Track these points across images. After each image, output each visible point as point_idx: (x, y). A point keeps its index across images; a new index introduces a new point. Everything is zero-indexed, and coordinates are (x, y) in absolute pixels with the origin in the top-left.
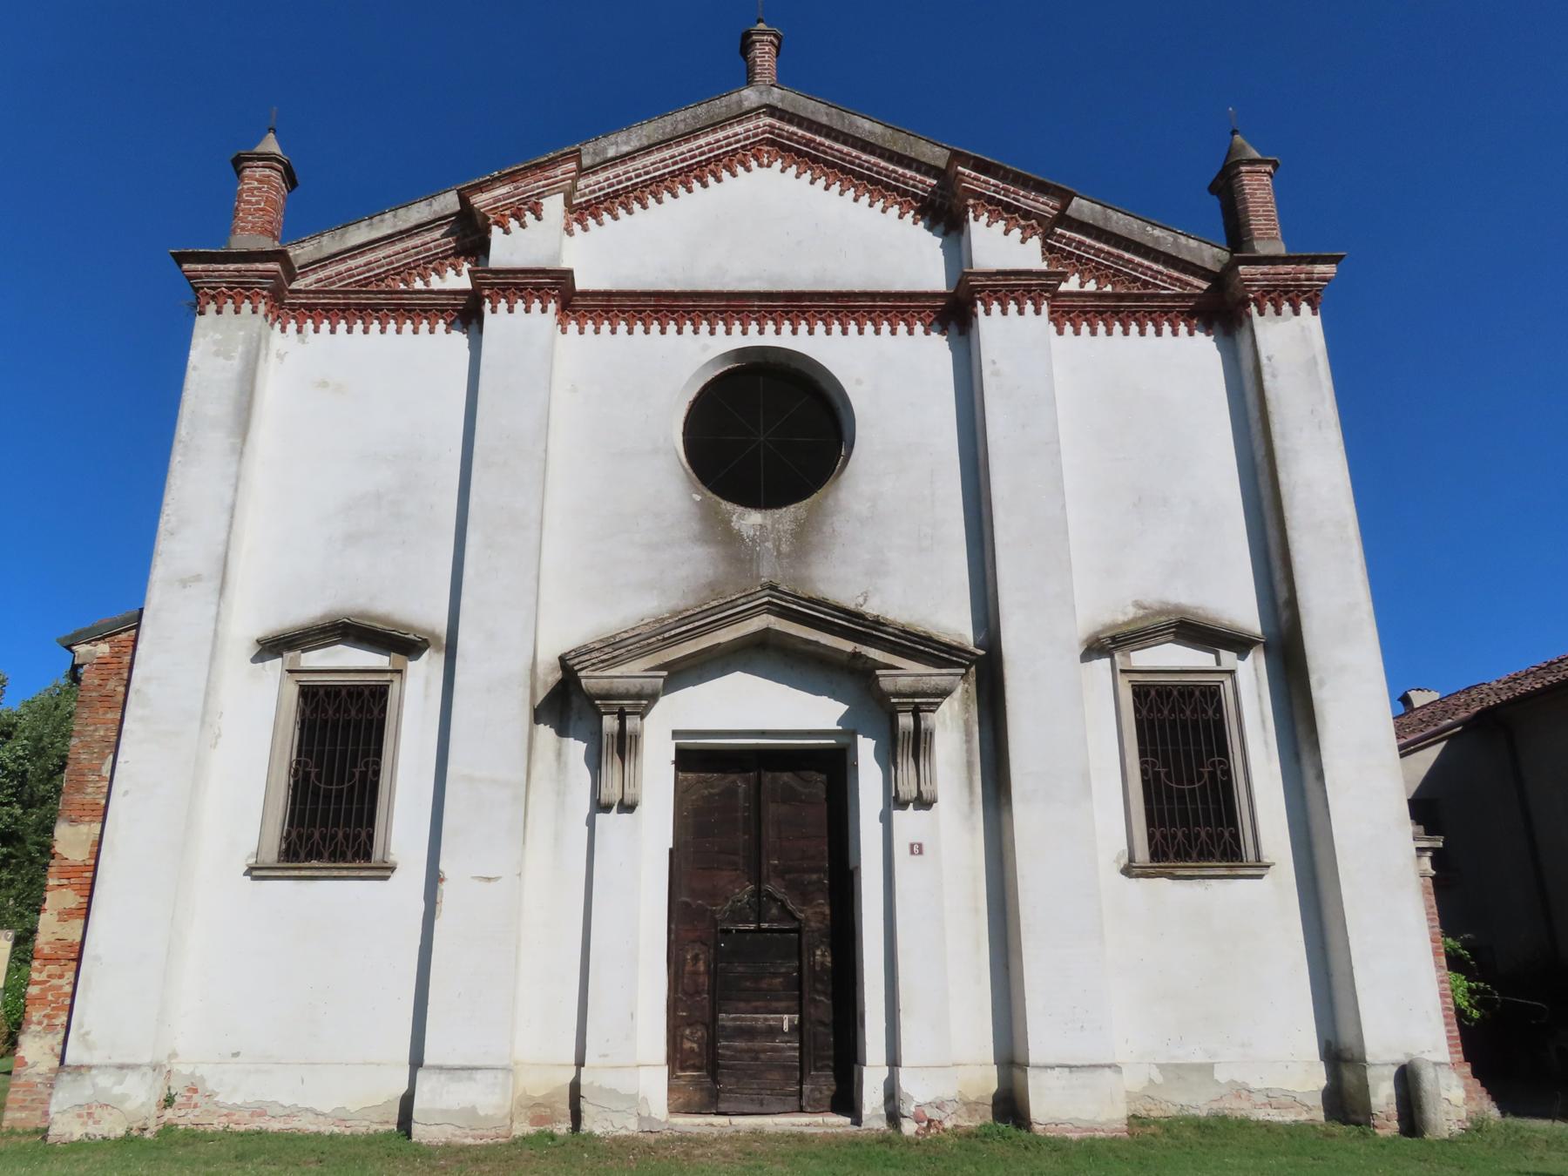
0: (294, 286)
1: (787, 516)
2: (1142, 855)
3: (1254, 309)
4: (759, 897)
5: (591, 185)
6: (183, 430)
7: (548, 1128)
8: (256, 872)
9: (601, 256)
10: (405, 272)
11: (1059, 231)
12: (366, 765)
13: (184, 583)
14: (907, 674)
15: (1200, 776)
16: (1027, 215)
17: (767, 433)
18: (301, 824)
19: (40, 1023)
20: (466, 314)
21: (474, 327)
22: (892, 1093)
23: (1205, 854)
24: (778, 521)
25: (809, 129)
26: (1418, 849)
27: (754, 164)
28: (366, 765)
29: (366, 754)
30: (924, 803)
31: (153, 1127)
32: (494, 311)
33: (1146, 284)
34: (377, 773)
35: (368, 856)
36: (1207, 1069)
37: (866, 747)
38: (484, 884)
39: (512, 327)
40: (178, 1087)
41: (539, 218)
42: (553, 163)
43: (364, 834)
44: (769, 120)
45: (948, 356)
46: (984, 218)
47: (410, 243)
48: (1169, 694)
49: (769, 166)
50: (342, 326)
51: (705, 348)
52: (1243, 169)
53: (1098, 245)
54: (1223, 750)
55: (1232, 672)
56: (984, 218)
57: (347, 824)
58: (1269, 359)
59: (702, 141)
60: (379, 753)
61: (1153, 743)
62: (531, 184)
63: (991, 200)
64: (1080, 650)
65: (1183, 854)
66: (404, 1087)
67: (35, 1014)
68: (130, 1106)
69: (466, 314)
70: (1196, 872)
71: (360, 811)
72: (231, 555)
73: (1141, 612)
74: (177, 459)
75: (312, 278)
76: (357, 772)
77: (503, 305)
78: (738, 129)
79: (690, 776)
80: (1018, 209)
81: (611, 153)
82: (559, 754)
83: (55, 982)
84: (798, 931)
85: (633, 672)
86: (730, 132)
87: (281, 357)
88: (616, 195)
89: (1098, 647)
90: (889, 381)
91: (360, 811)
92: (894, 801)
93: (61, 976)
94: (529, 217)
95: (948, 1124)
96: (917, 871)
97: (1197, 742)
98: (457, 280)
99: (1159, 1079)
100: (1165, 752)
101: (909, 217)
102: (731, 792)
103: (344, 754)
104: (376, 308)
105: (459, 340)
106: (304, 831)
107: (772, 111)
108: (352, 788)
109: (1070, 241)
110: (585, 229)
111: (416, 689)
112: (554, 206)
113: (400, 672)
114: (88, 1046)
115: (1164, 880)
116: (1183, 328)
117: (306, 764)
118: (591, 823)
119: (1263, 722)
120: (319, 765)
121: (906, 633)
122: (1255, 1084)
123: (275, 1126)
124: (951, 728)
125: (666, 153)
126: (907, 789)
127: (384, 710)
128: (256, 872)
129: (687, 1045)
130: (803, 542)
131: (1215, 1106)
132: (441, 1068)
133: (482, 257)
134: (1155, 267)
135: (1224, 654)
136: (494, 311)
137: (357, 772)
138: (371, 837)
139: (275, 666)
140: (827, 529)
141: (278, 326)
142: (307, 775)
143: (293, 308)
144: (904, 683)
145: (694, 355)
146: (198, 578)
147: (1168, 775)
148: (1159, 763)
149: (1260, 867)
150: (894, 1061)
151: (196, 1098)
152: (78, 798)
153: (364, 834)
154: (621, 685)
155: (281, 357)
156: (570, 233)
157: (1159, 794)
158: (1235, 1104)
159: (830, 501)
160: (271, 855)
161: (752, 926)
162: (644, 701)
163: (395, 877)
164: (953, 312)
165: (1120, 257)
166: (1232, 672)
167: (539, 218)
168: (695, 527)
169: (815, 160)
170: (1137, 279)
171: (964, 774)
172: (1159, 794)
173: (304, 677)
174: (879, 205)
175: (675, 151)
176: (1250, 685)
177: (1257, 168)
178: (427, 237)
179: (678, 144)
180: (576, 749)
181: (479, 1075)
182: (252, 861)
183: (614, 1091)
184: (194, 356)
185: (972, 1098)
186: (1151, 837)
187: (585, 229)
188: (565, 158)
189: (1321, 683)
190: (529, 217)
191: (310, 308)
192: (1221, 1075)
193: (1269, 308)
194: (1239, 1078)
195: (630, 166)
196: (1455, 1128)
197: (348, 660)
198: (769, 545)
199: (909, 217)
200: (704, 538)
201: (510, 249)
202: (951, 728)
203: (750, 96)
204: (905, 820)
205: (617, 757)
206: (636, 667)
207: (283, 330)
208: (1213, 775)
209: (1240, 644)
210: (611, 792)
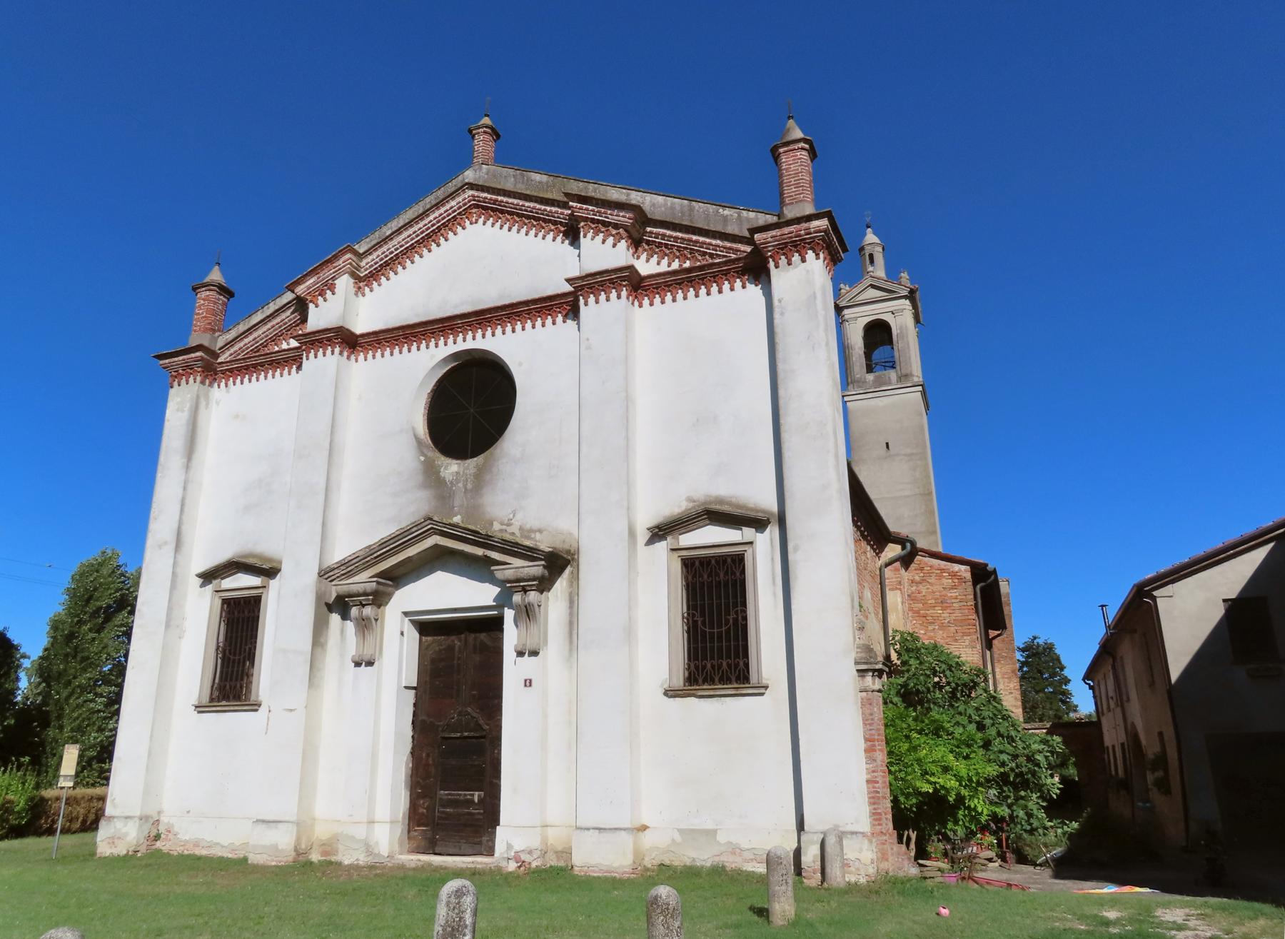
0: (219, 360)
1: (472, 463)
3: (772, 264)
5: (367, 263)
6: (162, 459)
7: (328, 858)
8: (671, 693)
9: (368, 311)
10: (275, 339)
11: (649, 229)
12: (736, 613)
13: (160, 547)
15: (727, 622)
16: (616, 226)
17: (472, 408)
18: (696, 659)
21: (763, 277)
23: (725, 680)
24: (467, 468)
25: (493, 193)
26: (858, 671)
28: (736, 613)
29: (735, 605)
31: (143, 849)
32: (586, 304)
33: (711, 256)
34: (745, 618)
35: (247, 699)
36: (712, 833)
37: (509, 615)
40: (162, 829)
42: (336, 257)
43: (741, 663)
44: (471, 192)
47: (274, 322)
48: (725, 561)
50: (726, 286)
51: (433, 356)
52: (781, 150)
53: (674, 234)
56: (590, 235)
57: (712, 658)
58: (780, 301)
59: (431, 218)
60: (744, 604)
62: (327, 273)
63: (593, 221)
65: (709, 680)
66: (796, 845)
68: (129, 839)
70: (712, 693)
71: (737, 647)
72: (184, 528)
73: (691, 505)
74: (159, 475)
75: (228, 353)
76: (731, 618)
77: (592, 299)
78: (453, 203)
79: (429, 638)
80: (609, 224)
81: (389, 233)
82: (342, 631)
86: (448, 206)
87: (217, 403)
88: (387, 264)
91: (737, 647)
95: (534, 865)
97: (727, 597)
99: (678, 838)
100: (703, 607)
101: (559, 239)
102: (450, 649)
103: (719, 606)
104: (262, 365)
105: (754, 291)
106: (233, 684)
107: (472, 186)
108: (728, 631)
109: (657, 235)
113: (751, 543)
114: (115, 806)
115: (693, 699)
116: (738, 283)
117: (694, 615)
119: (774, 579)
120: (703, 615)
122: (745, 845)
123: (204, 852)
125: (411, 231)
127: (743, 572)
128: (200, 708)
129: (421, 810)
130: (479, 481)
131: (717, 859)
134: (714, 242)
136: (586, 304)
137: (731, 618)
138: (747, 665)
139: (662, 547)
140: (494, 470)
141: (636, 303)
142: (695, 622)
143: (223, 372)
145: (424, 364)
146: (166, 543)
147: (704, 623)
148: (698, 614)
149: (761, 689)
151: (170, 836)
153: (741, 663)
154: (355, 588)
155: (217, 403)
158: (731, 858)
159: (498, 451)
163: (261, 709)
165: (690, 240)
168: (420, 478)
169: (502, 212)
170: (704, 254)
171: (567, 629)
173: (223, 594)
175: (416, 228)
177: (791, 147)
178: (283, 316)
179: (417, 223)
180: (350, 626)
181: (280, 825)
182: (666, 686)
183: (353, 837)
184: (169, 413)
185: (560, 849)
188: (343, 252)
189: (796, 549)
191: (231, 370)
192: (721, 838)
194: (734, 839)
195: (391, 244)
196: (863, 880)
198: (460, 485)
199: (559, 239)
200: (425, 486)
201: (320, 317)
203: (469, 175)
206: (364, 576)
207: (641, 306)
208: (736, 620)
209: (759, 523)
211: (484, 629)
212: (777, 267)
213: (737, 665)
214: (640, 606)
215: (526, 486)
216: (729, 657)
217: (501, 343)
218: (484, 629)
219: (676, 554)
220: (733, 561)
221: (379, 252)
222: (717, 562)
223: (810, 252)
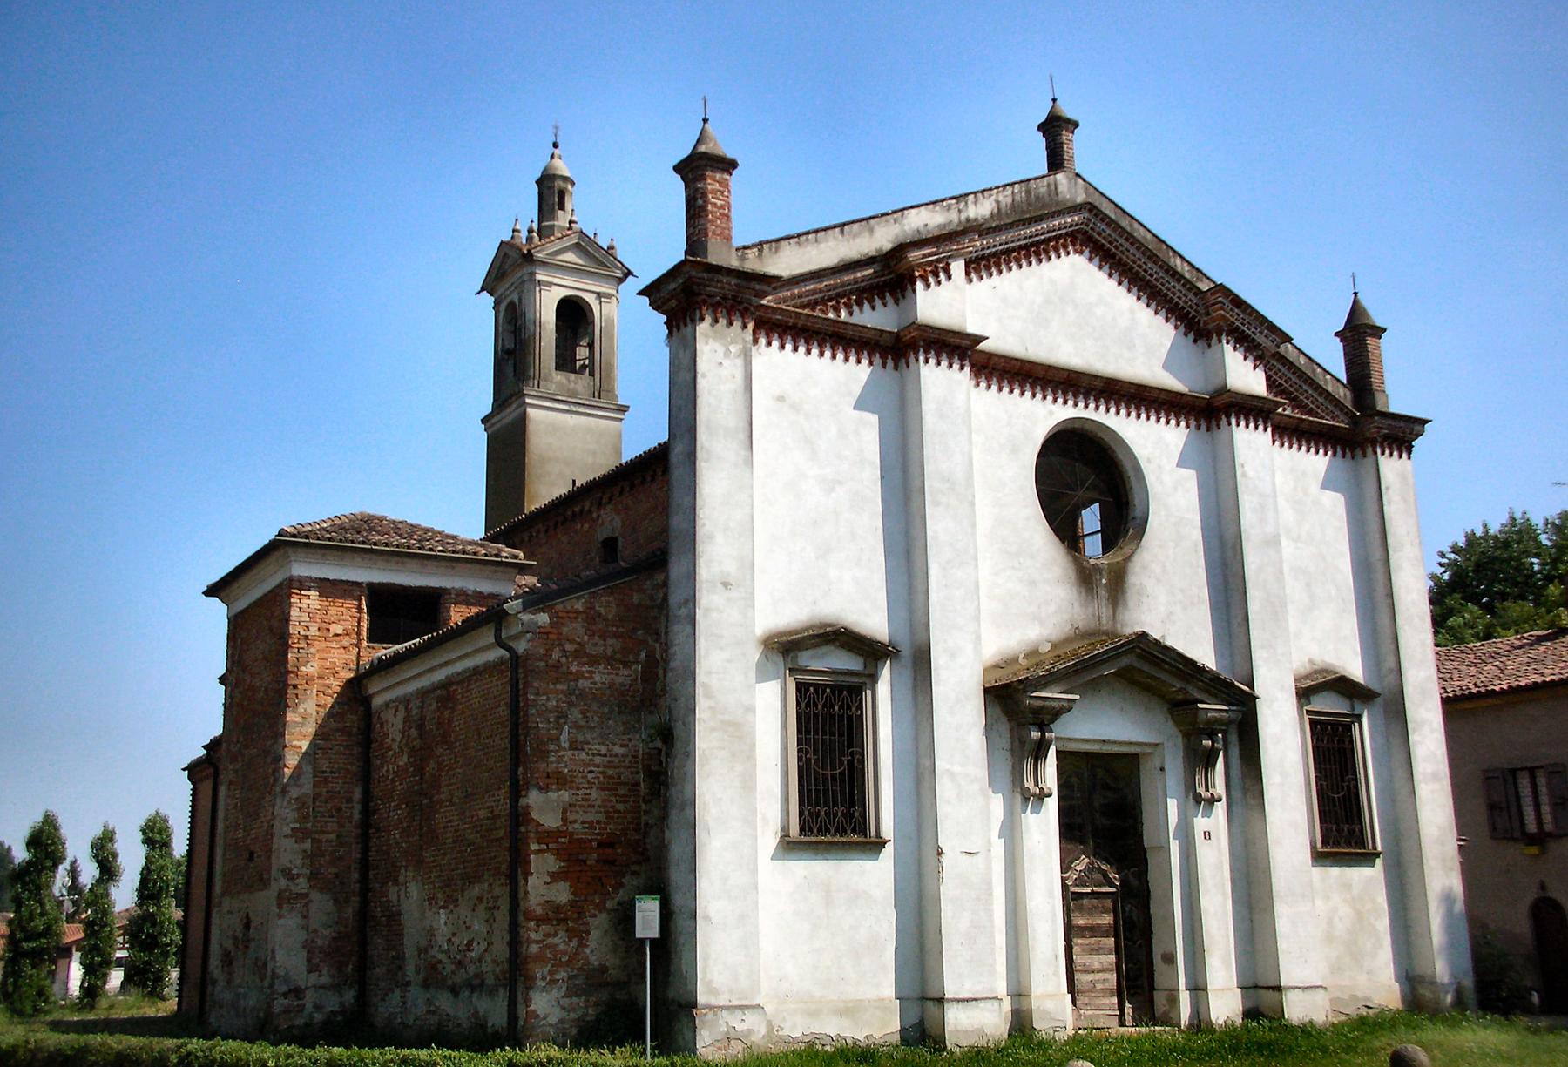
19: (544, 979)
29: (850, 745)
61: (808, 732)
67: (540, 971)
69: (901, 348)
83: (550, 940)
93: (556, 935)
96: (1198, 847)
98: (876, 317)
112: (958, 267)
132: (958, 1001)
152: (542, 766)
157: (809, 776)
164: (1209, 411)
167: (949, 278)
172: (809, 776)
186: (801, 814)
190: (942, 276)
197: (1329, 704)
208: (851, 763)
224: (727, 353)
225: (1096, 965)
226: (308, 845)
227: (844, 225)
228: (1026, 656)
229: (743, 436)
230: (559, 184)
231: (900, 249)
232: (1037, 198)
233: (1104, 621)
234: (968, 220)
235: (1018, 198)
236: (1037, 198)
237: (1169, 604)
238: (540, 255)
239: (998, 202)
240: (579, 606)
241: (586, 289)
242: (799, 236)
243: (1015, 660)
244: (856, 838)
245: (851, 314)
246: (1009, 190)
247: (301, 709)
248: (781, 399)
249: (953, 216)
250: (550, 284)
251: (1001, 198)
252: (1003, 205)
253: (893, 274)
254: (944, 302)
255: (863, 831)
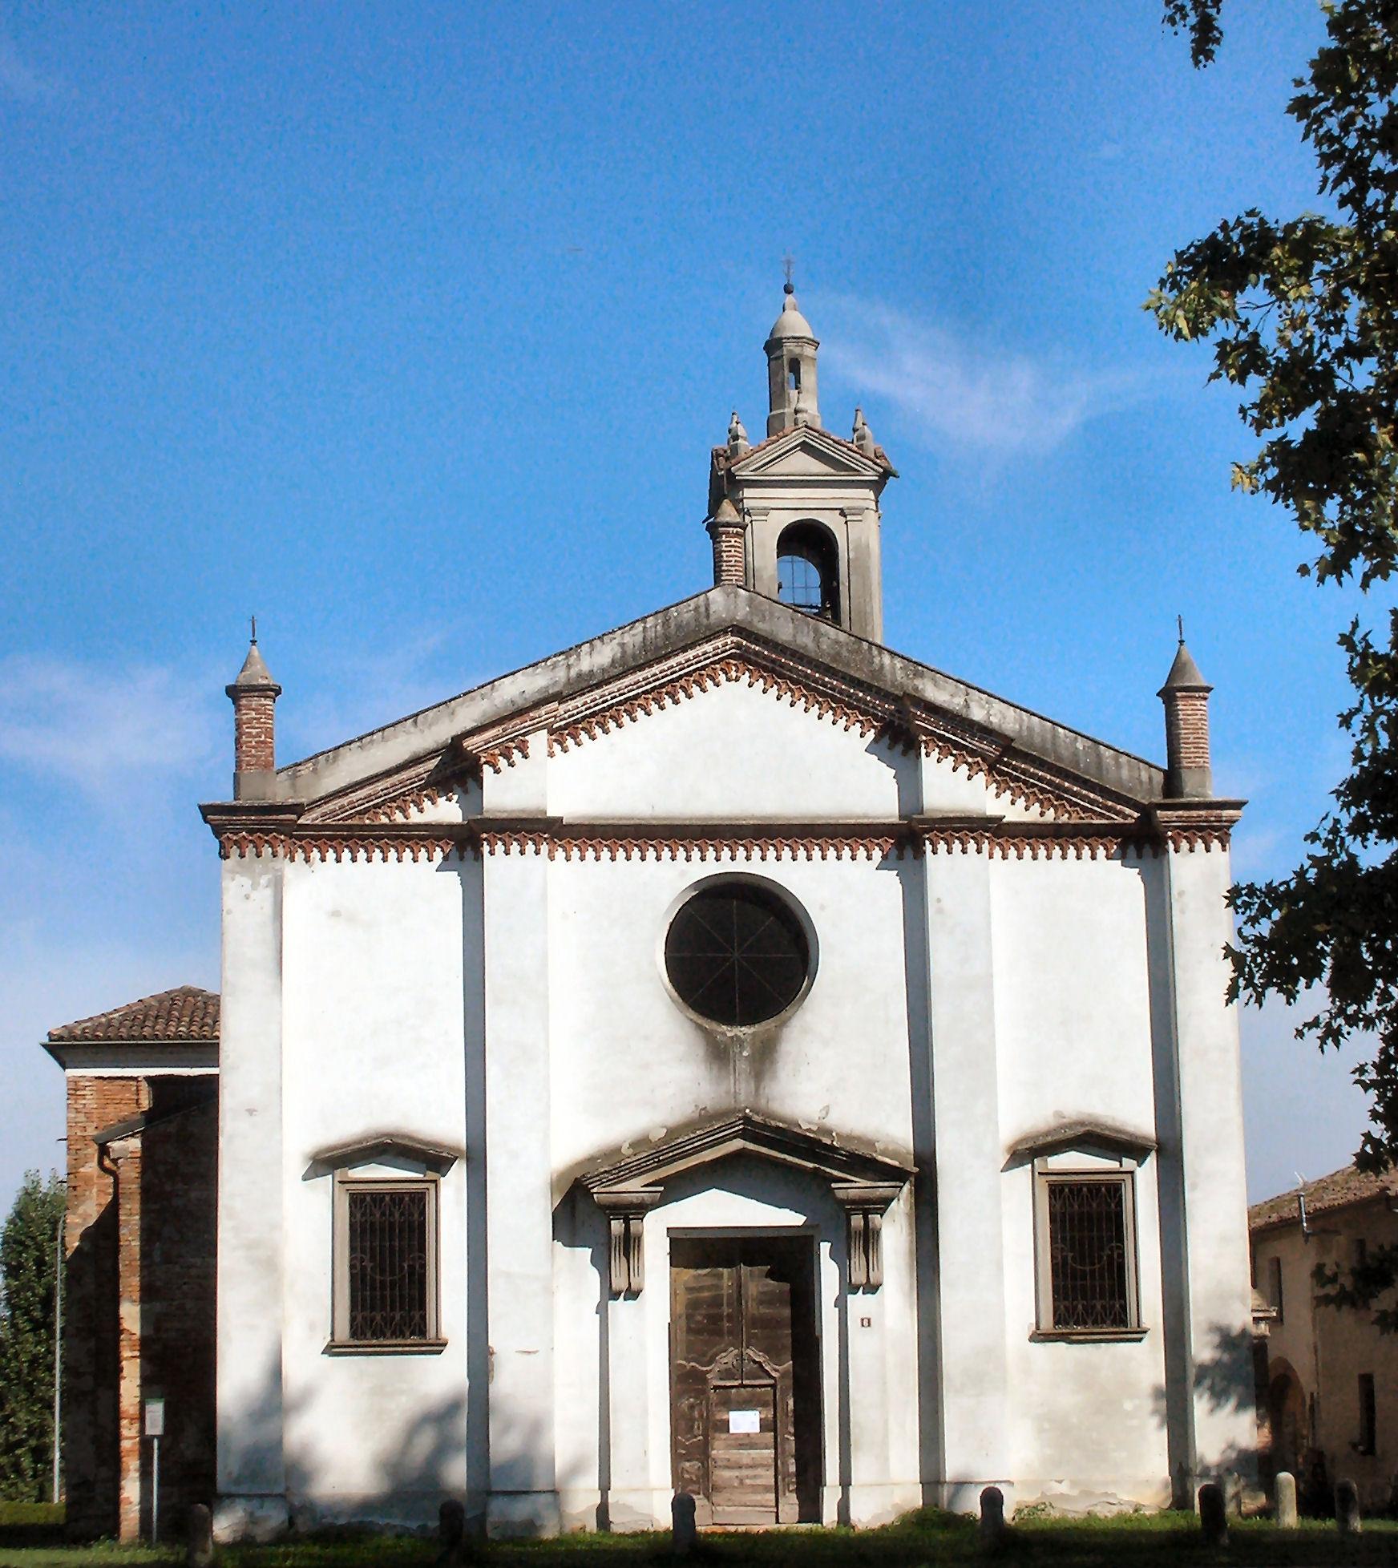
2: (1047, 1324)
3: (1171, 846)
4: (743, 1360)
12: (1111, 1249)
14: (857, 1187)
15: (1100, 1258)
20: (465, 845)
22: (844, 1507)
23: (398, 1332)
27: (722, 677)
30: (872, 1288)
38: (526, 1356)
39: (503, 866)
41: (525, 757)
43: (417, 1317)
44: (735, 639)
45: (898, 888)
46: (935, 754)
48: (402, 1200)
49: (737, 679)
51: (683, 874)
54: (1120, 1238)
55: (1132, 1173)
56: (935, 754)
58: (1181, 894)
64: (1003, 1158)
69: (465, 845)
84: (773, 1386)
85: (634, 1187)
89: (1026, 1153)
90: (844, 901)
92: (848, 1287)
94: (517, 755)
96: (868, 1334)
98: (447, 811)
100: (372, 1249)
108: (1102, 1269)
110: (565, 750)
111: (451, 1194)
118: (602, 1310)
121: (852, 1155)
124: (895, 1232)
126: (858, 1277)
130: (765, 1056)
133: (471, 783)
135: (1124, 1160)
138: (423, 1318)
144: (853, 1193)
145: (669, 880)
149: (438, 1347)
150: (845, 1482)
156: (551, 755)
160: (343, 1333)
161: (736, 1383)
162: (641, 1209)
163: (447, 1350)
164: (907, 840)
166: (1132, 1173)
173: (348, 1186)
174: (842, 722)
176: (1146, 1176)
186: (353, 1319)
187: (565, 750)
189: (1194, 1186)
190: (517, 755)
193: (1184, 845)
202: (895, 1232)
204: (858, 1303)
205: (623, 1259)
208: (1110, 1257)
210: (619, 1283)
211: (786, 1259)
212: (1176, 851)
213: (412, 1319)
214: (997, 1237)
215: (834, 1070)
216: (383, 1309)
217: (793, 873)
218: (786, 1259)
219: (1045, 1178)
220: (412, 1200)
221: (583, 699)
222: (392, 1200)
223: (1216, 841)
224: (255, 886)
225: (745, 1461)
226: (92, 1344)
227: (417, 715)
228: (631, 1146)
229: (272, 965)
230: (790, 348)
231: (458, 740)
232: (679, 627)
233: (742, 1097)
234: (579, 675)
235: (651, 634)
236: (679, 627)
237: (834, 1070)
238: (745, 474)
239: (622, 645)
240: (172, 1128)
241: (818, 504)
242: (361, 739)
243: (617, 1150)
244: (415, 1339)
245: (421, 811)
246: (639, 627)
247: (81, 1210)
248: (336, 914)
249: (561, 674)
250: (765, 511)
251: (627, 639)
252: (629, 650)
253: (457, 768)
254: (504, 790)
255: (422, 1331)
